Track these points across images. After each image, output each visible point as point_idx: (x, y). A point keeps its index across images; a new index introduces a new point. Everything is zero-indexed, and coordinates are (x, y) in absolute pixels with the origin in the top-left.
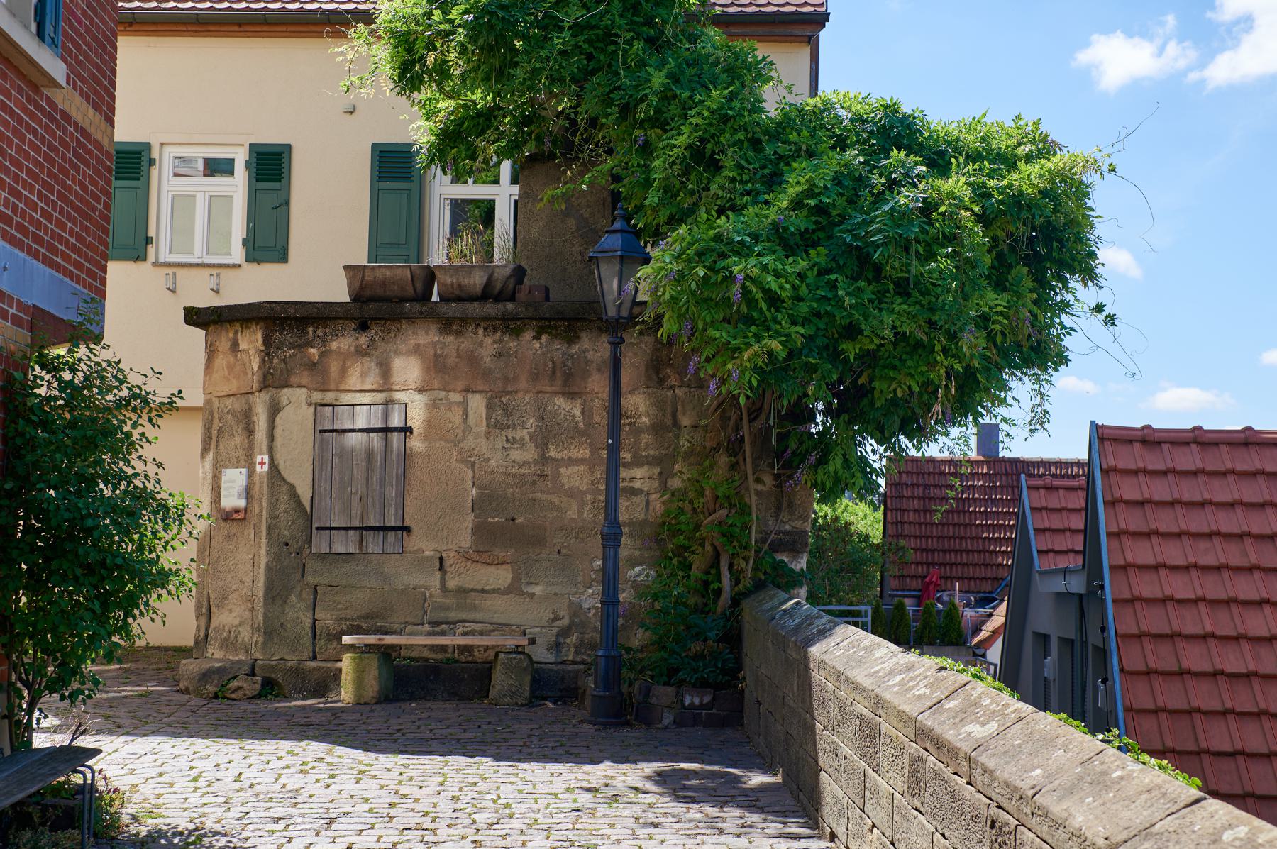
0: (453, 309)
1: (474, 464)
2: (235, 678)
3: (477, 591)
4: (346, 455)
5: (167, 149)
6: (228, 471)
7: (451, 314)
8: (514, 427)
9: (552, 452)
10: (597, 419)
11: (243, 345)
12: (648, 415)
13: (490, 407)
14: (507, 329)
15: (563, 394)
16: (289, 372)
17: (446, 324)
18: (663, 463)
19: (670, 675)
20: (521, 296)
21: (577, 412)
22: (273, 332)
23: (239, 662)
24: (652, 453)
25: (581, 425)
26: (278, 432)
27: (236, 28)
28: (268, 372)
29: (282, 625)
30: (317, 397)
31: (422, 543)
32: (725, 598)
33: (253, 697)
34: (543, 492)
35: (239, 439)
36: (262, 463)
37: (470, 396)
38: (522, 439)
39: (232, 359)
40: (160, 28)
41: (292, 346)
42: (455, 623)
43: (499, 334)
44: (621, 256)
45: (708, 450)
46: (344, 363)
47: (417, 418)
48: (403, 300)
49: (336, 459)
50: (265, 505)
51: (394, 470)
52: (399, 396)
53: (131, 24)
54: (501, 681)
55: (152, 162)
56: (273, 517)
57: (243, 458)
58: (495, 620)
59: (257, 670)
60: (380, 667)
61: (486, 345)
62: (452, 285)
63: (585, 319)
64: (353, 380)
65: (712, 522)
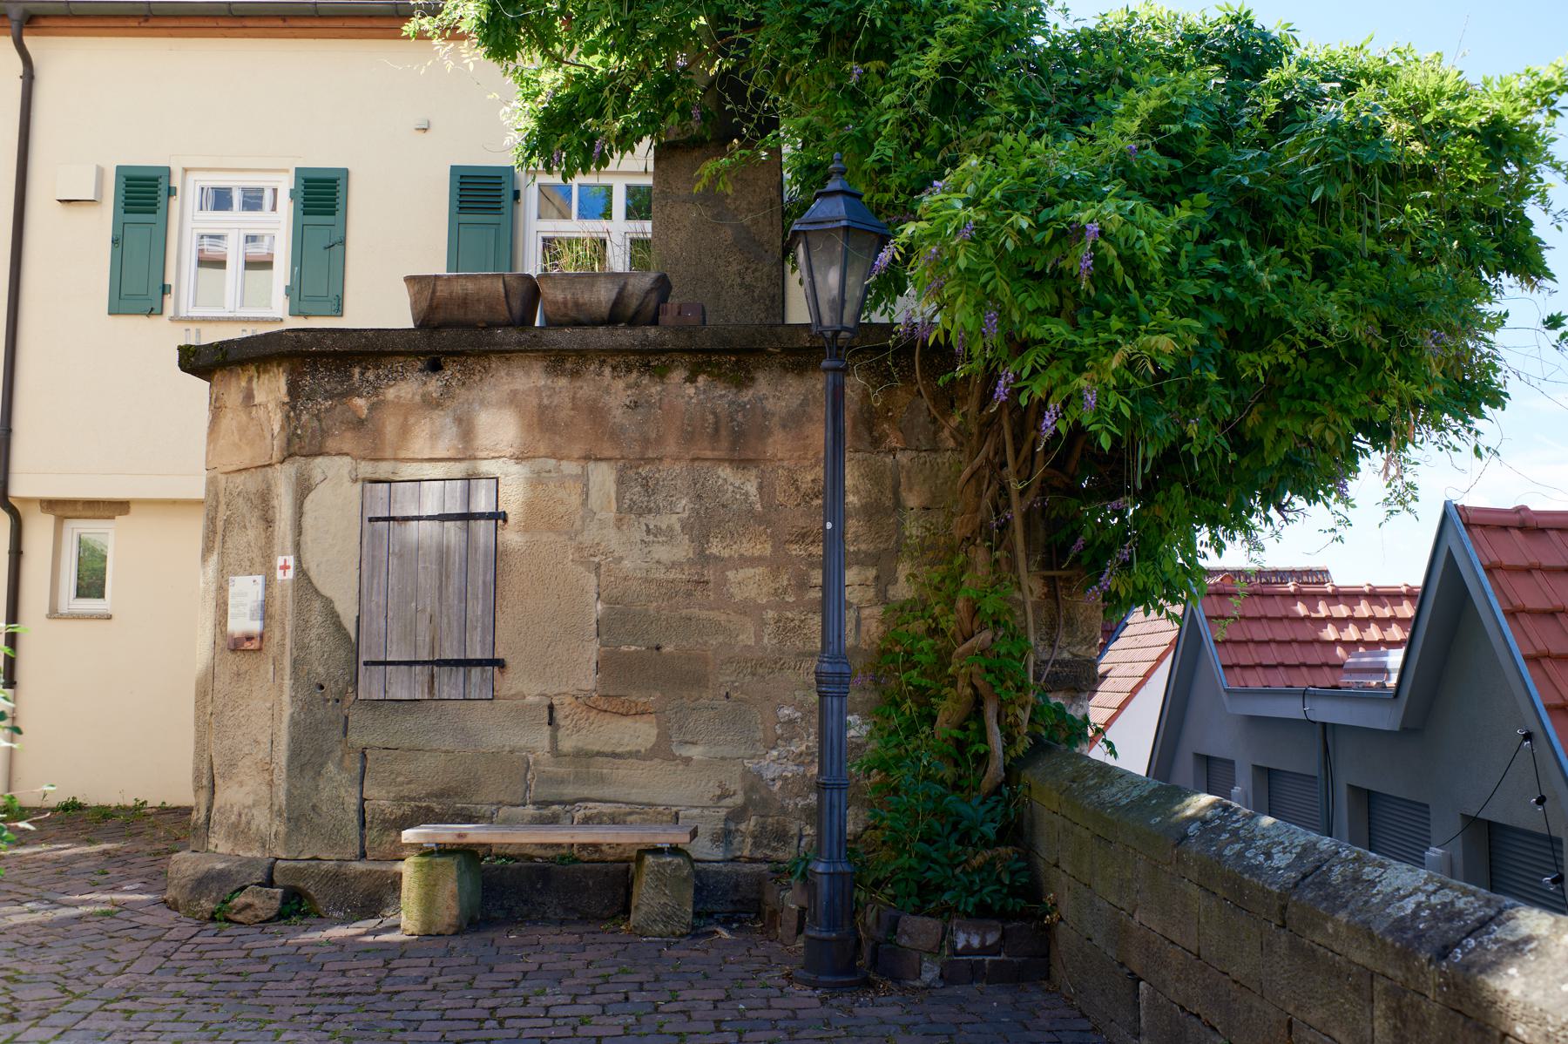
0: (565, 338)
1: (598, 566)
2: (242, 889)
3: (605, 755)
4: (408, 555)
5: (191, 177)
6: (237, 578)
7: (564, 345)
8: (658, 511)
9: (715, 548)
10: (781, 498)
11: (259, 397)
12: (857, 492)
13: (621, 482)
14: (647, 368)
15: (731, 461)
16: (325, 433)
17: (558, 360)
18: (882, 562)
19: (925, 895)
20: (667, 318)
21: (752, 488)
22: (302, 374)
23: (251, 862)
24: (863, 547)
25: (758, 507)
26: (308, 521)
27: (280, 23)
28: (294, 434)
29: (314, 807)
30: (366, 469)
31: (521, 684)
32: (996, 768)
33: (269, 920)
34: (701, 607)
35: (253, 533)
36: (285, 568)
37: (591, 465)
38: (670, 528)
39: (244, 418)
40: (184, 23)
41: (330, 396)
42: (572, 803)
43: (635, 374)
44: (846, 228)
45: (958, 541)
46: (406, 419)
47: (513, 499)
48: (491, 325)
49: (393, 561)
50: (288, 628)
51: (481, 575)
52: (486, 467)
53: (147, 18)
54: (647, 898)
55: (171, 192)
56: (301, 646)
57: (258, 560)
58: (633, 798)
59: (277, 877)
60: (460, 879)
61: (614, 391)
62: (565, 303)
63: (762, 351)
64: (419, 444)
65: (971, 651)
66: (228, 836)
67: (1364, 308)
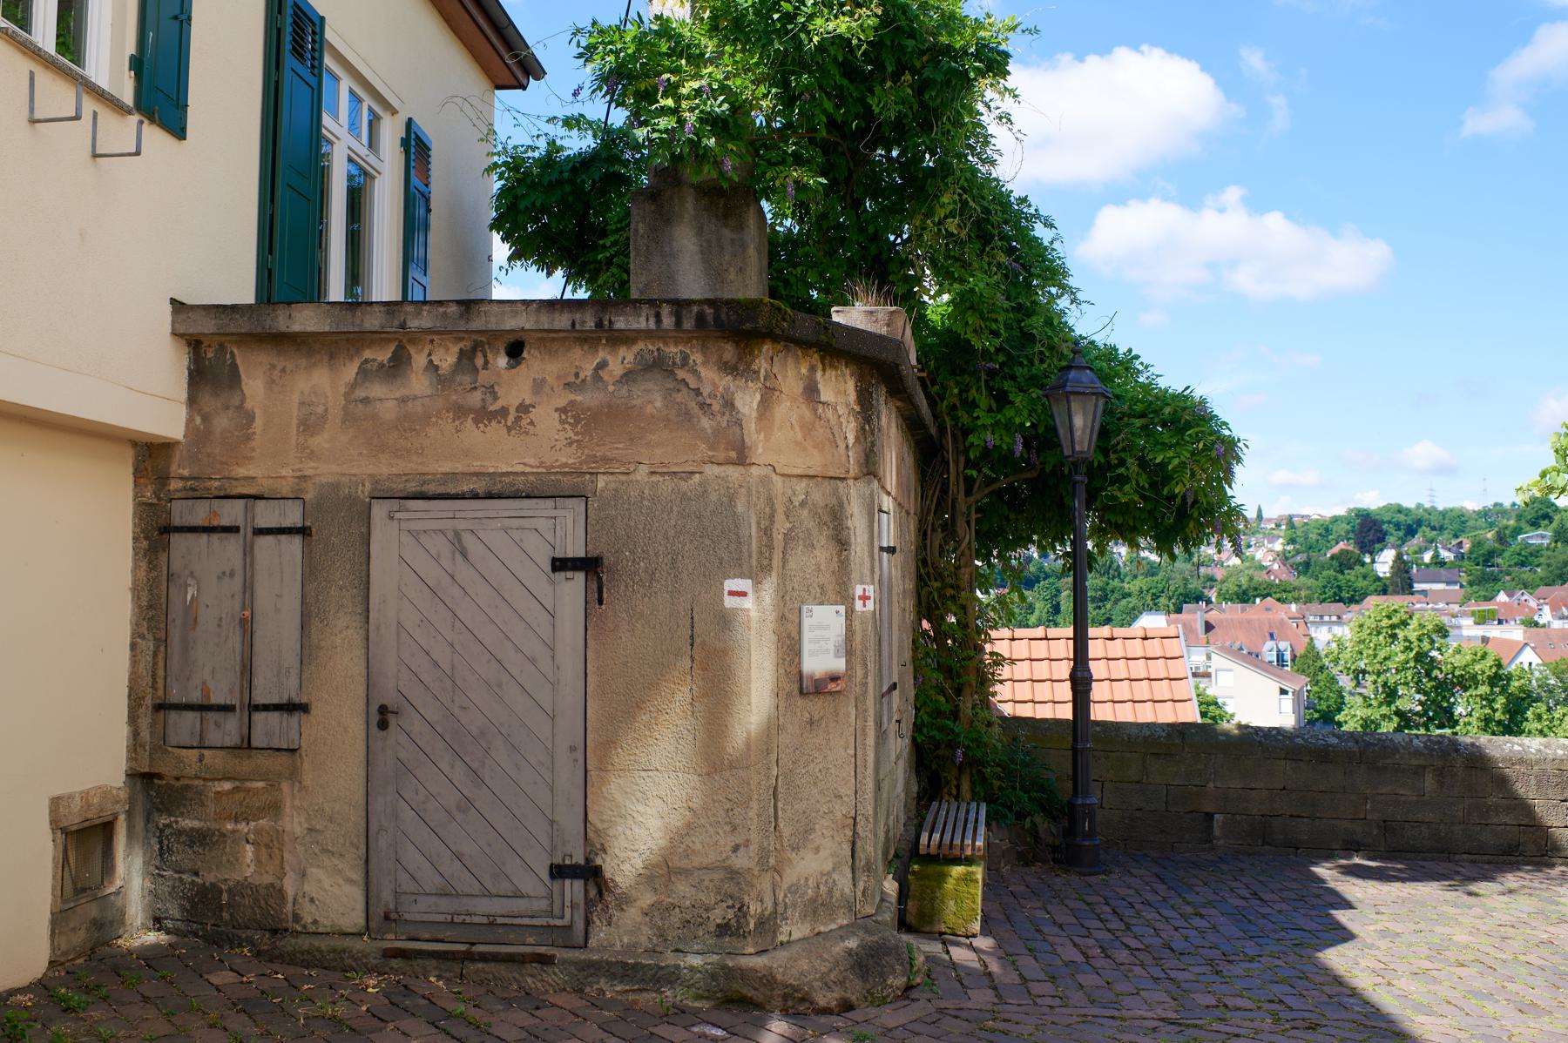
6: (816, 608)
11: (826, 395)
35: (823, 554)
36: (864, 598)
39: (807, 414)
57: (830, 588)
66: (804, 917)
67: (809, 161)
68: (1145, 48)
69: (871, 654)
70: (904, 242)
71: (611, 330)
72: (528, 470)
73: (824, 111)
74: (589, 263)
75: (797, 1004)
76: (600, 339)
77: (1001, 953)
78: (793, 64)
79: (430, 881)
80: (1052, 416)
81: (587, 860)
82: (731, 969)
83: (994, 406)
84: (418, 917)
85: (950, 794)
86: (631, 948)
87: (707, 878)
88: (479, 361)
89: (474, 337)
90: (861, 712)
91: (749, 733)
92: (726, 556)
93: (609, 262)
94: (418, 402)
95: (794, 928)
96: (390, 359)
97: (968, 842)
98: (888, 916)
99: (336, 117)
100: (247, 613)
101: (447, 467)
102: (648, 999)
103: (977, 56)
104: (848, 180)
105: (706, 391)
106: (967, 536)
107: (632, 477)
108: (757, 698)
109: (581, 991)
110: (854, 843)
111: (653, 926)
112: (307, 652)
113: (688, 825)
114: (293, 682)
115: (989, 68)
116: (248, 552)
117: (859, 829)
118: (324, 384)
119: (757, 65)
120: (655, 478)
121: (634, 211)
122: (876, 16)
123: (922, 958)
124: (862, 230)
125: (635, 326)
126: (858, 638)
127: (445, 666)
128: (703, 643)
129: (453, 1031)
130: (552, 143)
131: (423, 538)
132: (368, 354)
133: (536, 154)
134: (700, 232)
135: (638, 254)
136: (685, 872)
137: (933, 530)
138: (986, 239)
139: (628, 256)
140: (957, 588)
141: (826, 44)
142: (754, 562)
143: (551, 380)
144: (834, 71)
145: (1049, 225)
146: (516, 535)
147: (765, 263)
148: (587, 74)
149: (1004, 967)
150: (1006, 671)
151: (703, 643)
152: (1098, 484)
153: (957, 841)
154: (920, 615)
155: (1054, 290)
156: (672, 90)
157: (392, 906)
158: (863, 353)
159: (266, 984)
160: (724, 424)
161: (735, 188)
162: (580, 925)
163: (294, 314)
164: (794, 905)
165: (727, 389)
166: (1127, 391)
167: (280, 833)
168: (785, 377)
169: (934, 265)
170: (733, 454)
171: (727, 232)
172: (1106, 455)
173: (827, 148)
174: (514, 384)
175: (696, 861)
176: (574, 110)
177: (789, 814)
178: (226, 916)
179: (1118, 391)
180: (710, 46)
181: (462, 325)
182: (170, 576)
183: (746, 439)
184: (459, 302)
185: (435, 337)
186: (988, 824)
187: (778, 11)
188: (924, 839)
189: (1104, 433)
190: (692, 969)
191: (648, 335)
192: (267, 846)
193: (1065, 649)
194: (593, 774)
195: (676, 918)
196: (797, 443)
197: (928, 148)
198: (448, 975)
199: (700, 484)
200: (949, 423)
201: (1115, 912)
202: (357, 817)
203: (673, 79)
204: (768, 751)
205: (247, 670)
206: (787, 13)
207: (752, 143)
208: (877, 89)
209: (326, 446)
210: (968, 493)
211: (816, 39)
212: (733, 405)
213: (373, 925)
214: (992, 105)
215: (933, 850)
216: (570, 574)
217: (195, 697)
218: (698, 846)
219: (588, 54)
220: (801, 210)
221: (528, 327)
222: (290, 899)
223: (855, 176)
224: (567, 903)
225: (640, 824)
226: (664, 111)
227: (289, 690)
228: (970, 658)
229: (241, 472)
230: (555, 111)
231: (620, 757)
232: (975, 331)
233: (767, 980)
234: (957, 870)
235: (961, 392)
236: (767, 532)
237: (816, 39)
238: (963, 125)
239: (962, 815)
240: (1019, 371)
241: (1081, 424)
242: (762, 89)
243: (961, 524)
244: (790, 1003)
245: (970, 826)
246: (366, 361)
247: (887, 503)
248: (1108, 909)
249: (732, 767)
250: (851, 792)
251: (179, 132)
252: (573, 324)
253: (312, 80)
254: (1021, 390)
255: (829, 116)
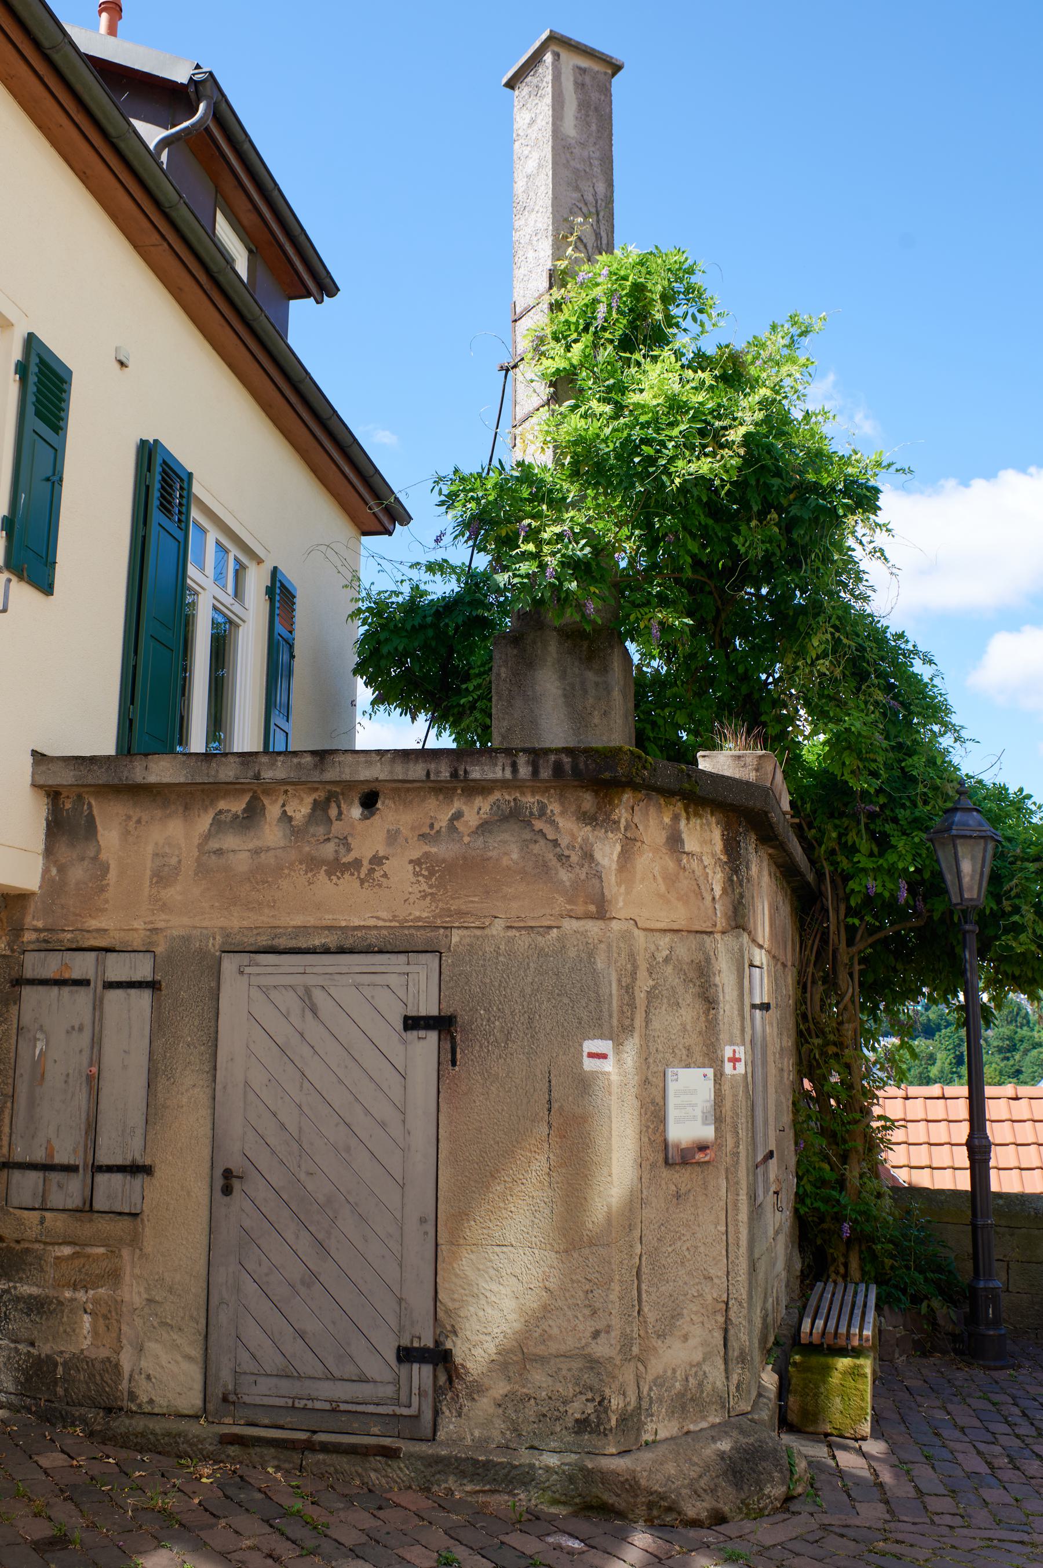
6: (682, 1072)
11: (691, 844)
35: (689, 1013)
36: (734, 1060)
39: (671, 865)
57: (697, 1050)
67: (674, 602)
68: (1032, 470)
69: (743, 1122)
70: (776, 682)
71: (466, 779)
72: (381, 923)
73: (688, 552)
74: (452, 707)
75: (663, 1514)
76: (455, 789)
77: (894, 1460)
78: (656, 507)
79: (272, 1360)
80: (937, 861)
81: (437, 1343)
82: (590, 1472)
83: (876, 850)
84: (258, 1401)
85: (837, 1273)
86: (481, 1444)
87: (564, 1367)
88: (333, 812)
89: (328, 787)
90: (732, 1185)
91: (609, 1207)
92: (584, 1015)
93: (473, 707)
94: (271, 853)
95: (660, 1426)
96: (245, 810)
97: (855, 1330)
98: (765, 1414)
99: (202, 569)
100: (94, 1069)
101: (298, 921)
102: (499, 1501)
103: (846, 493)
104: (716, 620)
105: (564, 842)
106: (850, 988)
107: (487, 931)
108: (618, 1166)
109: (428, 1490)
110: (726, 1331)
111: (506, 1419)
112: (153, 1112)
113: (545, 1307)
114: (137, 1143)
115: (859, 504)
116: (98, 1006)
117: (732, 1314)
118: (177, 834)
119: (620, 507)
120: (511, 933)
121: (496, 655)
122: (739, 456)
123: (803, 1464)
124: (732, 669)
125: (491, 776)
126: (728, 1104)
127: (293, 1128)
128: (561, 1107)
129: (288, 1531)
130: (415, 588)
131: (274, 995)
132: (222, 805)
133: (400, 599)
134: (563, 675)
135: (500, 698)
136: (541, 1360)
137: (813, 982)
138: (862, 677)
139: (490, 700)
140: (840, 1045)
141: (688, 486)
142: (615, 1022)
143: (405, 831)
144: (698, 511)
145: (929, 661)
146: (367, 992)
147: (631, 705)
148: (449, 520)
149: (897, 1476)
150: (897, 1135)
151: (561, 1107)
152: (990, 932)
153: (843, 1330)
154: (800, 1075)
155: (936, 728)
156: (533, 535)
157: (230, 1387)
158: (729, 801)
159: (96, 1469)
160: (583, 877)
161: (598, 630)
162: (428, 1415)
163: (151, 765)
164: (660, 1400)
165: (586, 840)
166: (1019, 833)
167: (119, 1303)
168: (647, 827)
169: (807, 704)
170: (592, 908)
171: (590, 675)
172: (999, 902)
173: (692, 588)
174: (368, 835)
175: (554, 1347)
176: (437, 556)
177: (654, 1297)
178: (60, 1391)
179: (1009, 833)
180: (572, 492)
181: (316, 776)
182: (19, 1029)
183: (606, 892)
184: (313, 753)
185: (289, 788)
186: (878, 1308)
187: (639, 455)
188: (806, 1326)
189: (995, 878)
190: (548, 1469)
191: (504, 784)
192: (105, 1317)
193: (961, 1109)
194: (443, 1248)
195: (531, 1410)
196: (660, 896)
197: (797, 586)
198: (287, 1466)
199: (558, 939)
200: (827, 868)
201: (1024, 1414)
202: (197, 1288)
203: (534, 524)
204: (631, 1228)
205: (92, 1128)
206: (649, 457)
207: (616, 585)
208: (743, 528)
209: (179, 898)
210: (850, 943)
211: (677, 481)
212: (592, 856)
213: (210, 1407)
214: (865, 540)
215: (816, 1339)
216: (422, 1033)
217: (39, 1156)
218: (555, 1331)
219: (449, 501)
220: (669, 651)
221: (382, 777)
222: (126, 1376)
223: (723, 615)
224: (415, 1391)
225: (493, 1304)
226: (525, 556)
227: (133, 1152)
228: (856, 1122)
229: (93, 924)
230: (418, 558)
231: (473, 1230)
232: (852, 772)
233: (630, 1485)
234: (844, 1363)
235: (840, 836)
236: (628, 990)
237: (677, 481)
238: (833, 562)
239: (849, 1299)
240: (901, 814)
241: (968, 871)
242: (625, 531)
243: (843, 977)
244: (655, 1513)
245: (858, 1312)
246: (221, 812)
247: (760, 957)
248: (1016, 1411)
249: (591, 1244)
250: (722, 1273)
251: (46, 587)
252: (428, 774)
253: (178, 534)
254: (904, 833)
255: (693, 556)
